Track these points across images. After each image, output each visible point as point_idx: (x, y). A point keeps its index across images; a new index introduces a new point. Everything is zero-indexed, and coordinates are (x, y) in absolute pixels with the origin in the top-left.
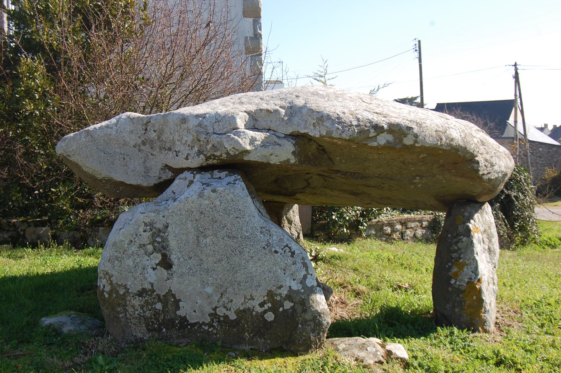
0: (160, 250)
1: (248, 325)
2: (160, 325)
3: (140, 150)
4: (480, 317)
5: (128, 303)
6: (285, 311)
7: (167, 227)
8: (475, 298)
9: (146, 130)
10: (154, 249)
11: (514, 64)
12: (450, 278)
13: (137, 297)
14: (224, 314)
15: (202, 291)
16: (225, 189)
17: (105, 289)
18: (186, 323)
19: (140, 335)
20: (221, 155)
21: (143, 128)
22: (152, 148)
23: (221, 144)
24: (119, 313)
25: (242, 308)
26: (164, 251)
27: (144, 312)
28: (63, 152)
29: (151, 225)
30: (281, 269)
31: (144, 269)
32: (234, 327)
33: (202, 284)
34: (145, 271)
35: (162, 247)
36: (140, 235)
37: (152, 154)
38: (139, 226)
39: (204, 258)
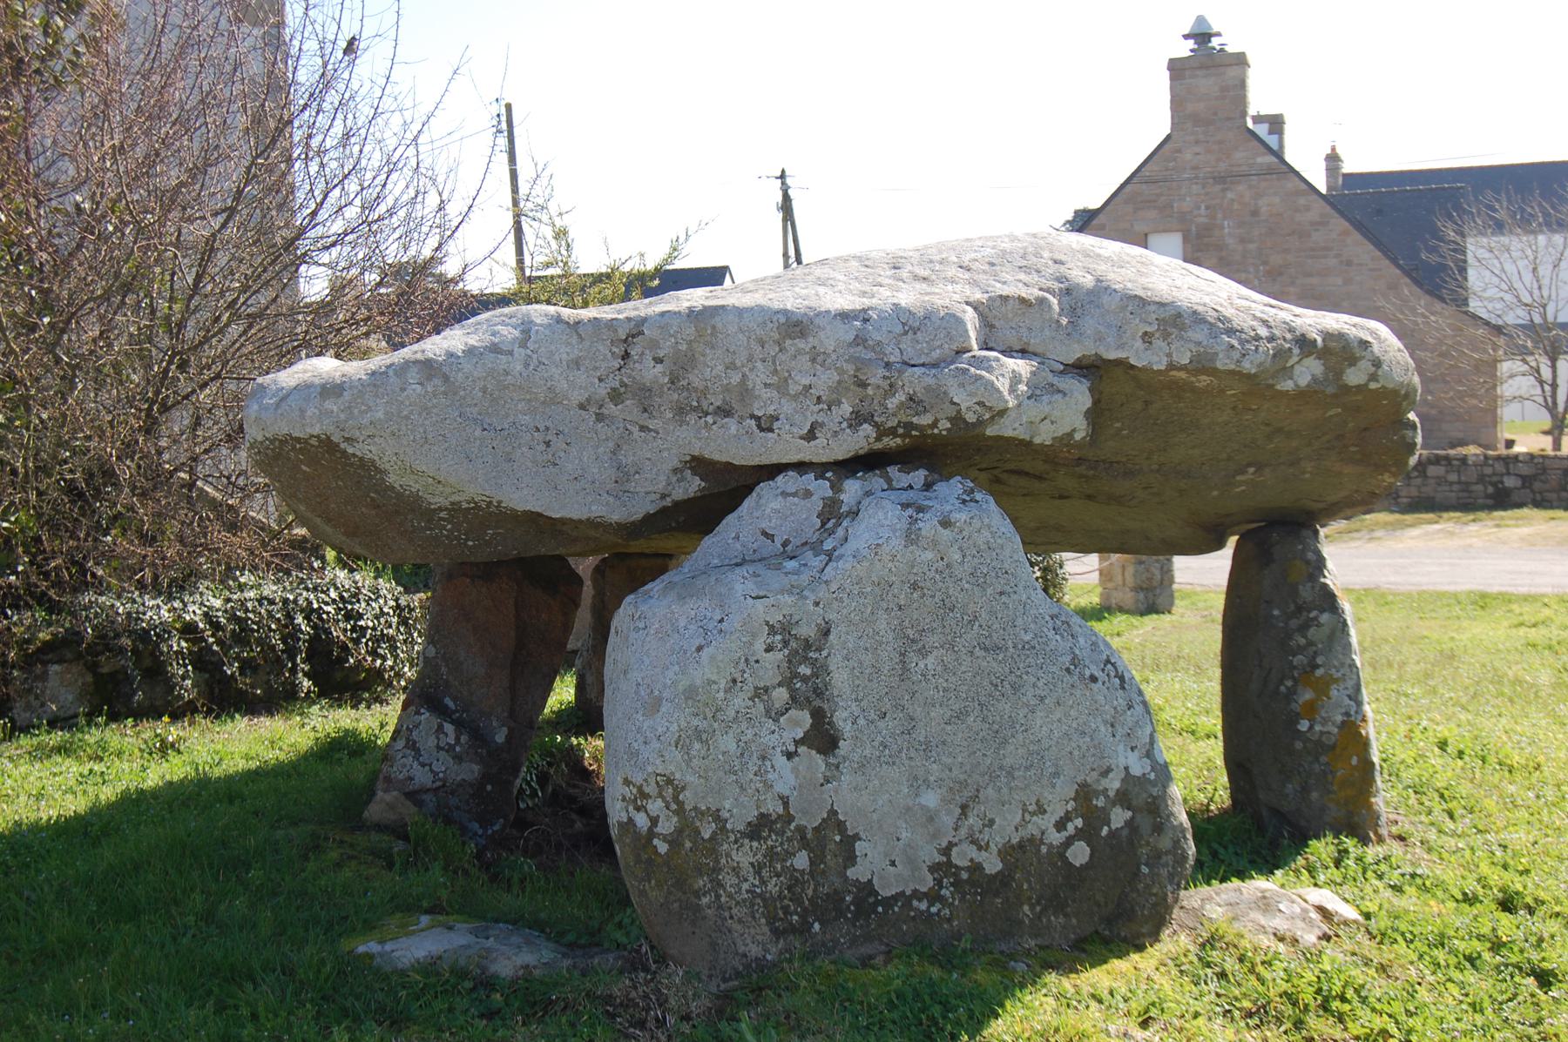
0: (807, 699)
1: (1029, 882)
2: (803, 917)
3: (600, 418)
4: (1369, 806)
5: (723, 861)
6: (1113, 834)
7: (827, 633)
8: (1354, 761)
9: (626, 356)
10: (793, 698)
11: (779, 174)
12: (1294, 718)
13: (746, 841)
14: (972, 860)
15: (911, 804)
16: (972, 518)
17: (658, 830)
18: (871, 900)
19: (754, 951)
20: (935, 424)
21: (613, 354)
22: (645, 410)
23: (939, 394)
24: (697, 894)
25: (1015, 841)
26: (817, 703)
27: (763, 882)
28: (331, 429)
29: (783, 630)
30: (1105, 722)
31: (763, 758)
32: (997, 895)
33: (912, 786)
34: (768, 763)
35: (815, 691)
36: (757, 661)
37: (643, 428)
38: (754, 636)
39: (918, 712)
